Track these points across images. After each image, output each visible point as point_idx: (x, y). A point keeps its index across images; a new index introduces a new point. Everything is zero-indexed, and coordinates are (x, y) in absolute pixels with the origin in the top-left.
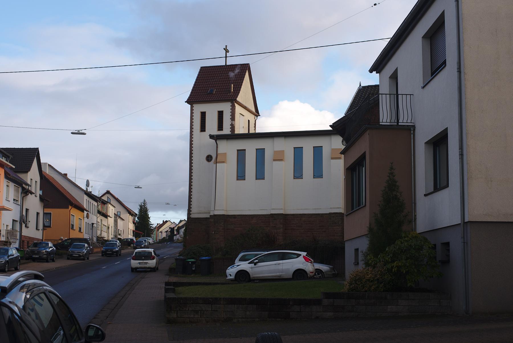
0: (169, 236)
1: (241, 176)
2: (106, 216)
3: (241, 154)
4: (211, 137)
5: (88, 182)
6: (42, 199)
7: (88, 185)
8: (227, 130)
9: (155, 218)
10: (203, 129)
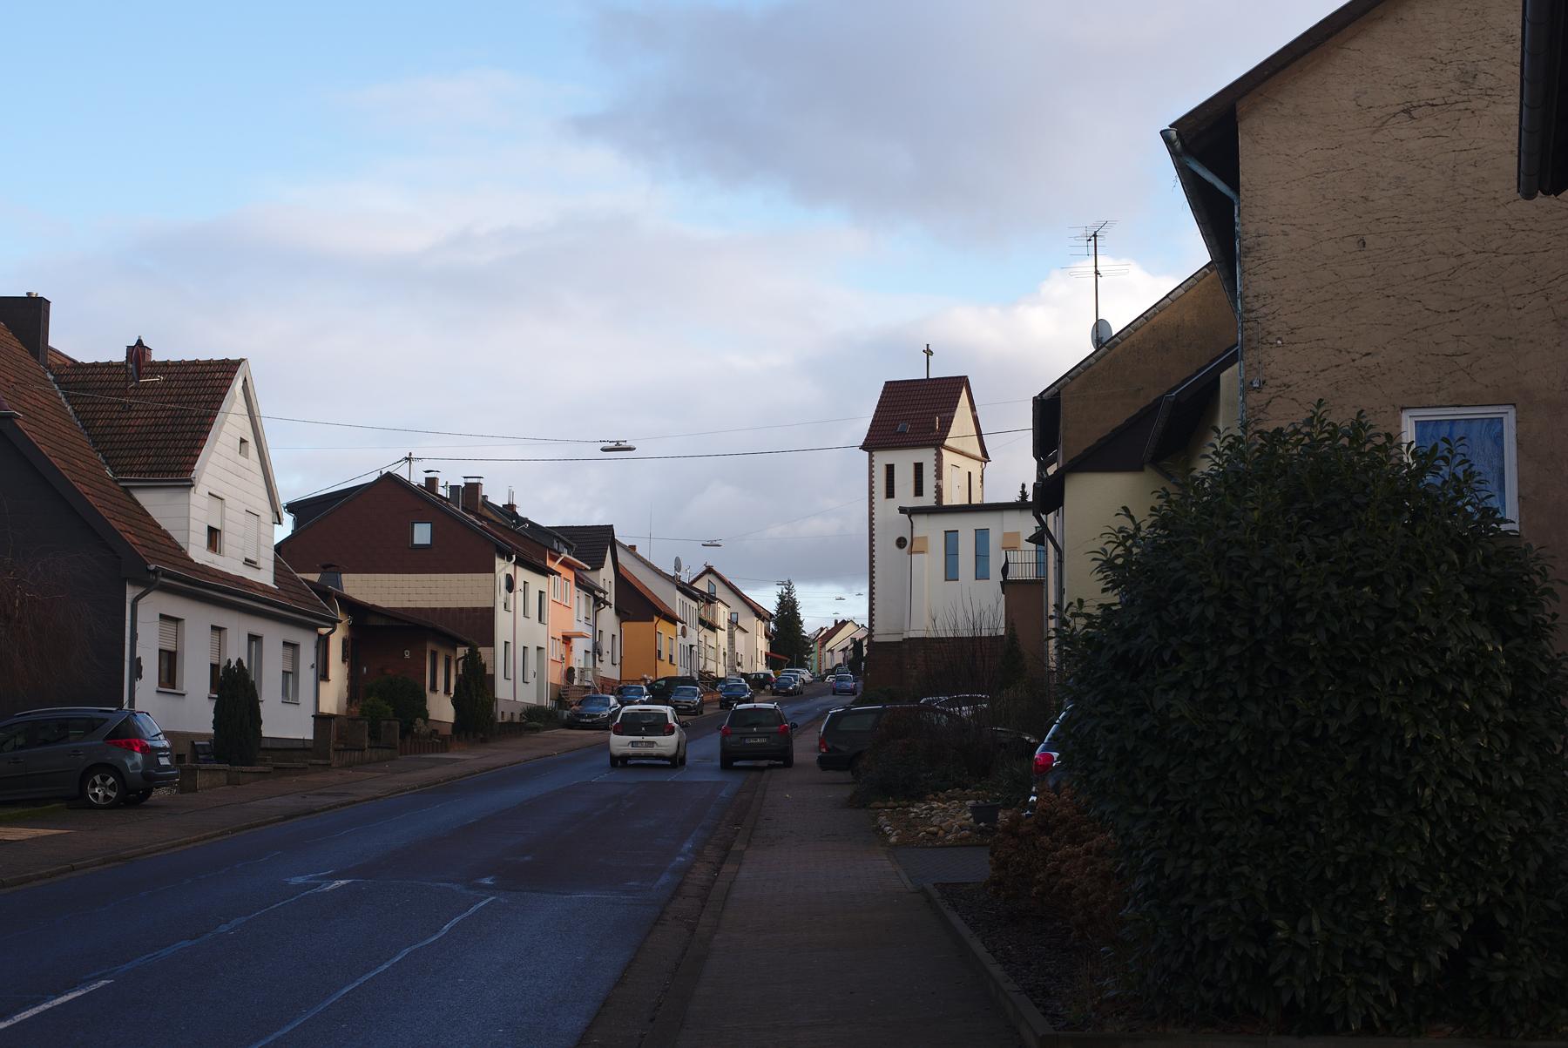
0: (850, 662)
1: (951, 573)
2: (713, 627)
3: (951, 537)
4: (902, 510)
5: (678, 561)
6: (618, 612)
7: (678, 567)
8: (928, 499)
9: (813, 619)
10: (890, 493)
